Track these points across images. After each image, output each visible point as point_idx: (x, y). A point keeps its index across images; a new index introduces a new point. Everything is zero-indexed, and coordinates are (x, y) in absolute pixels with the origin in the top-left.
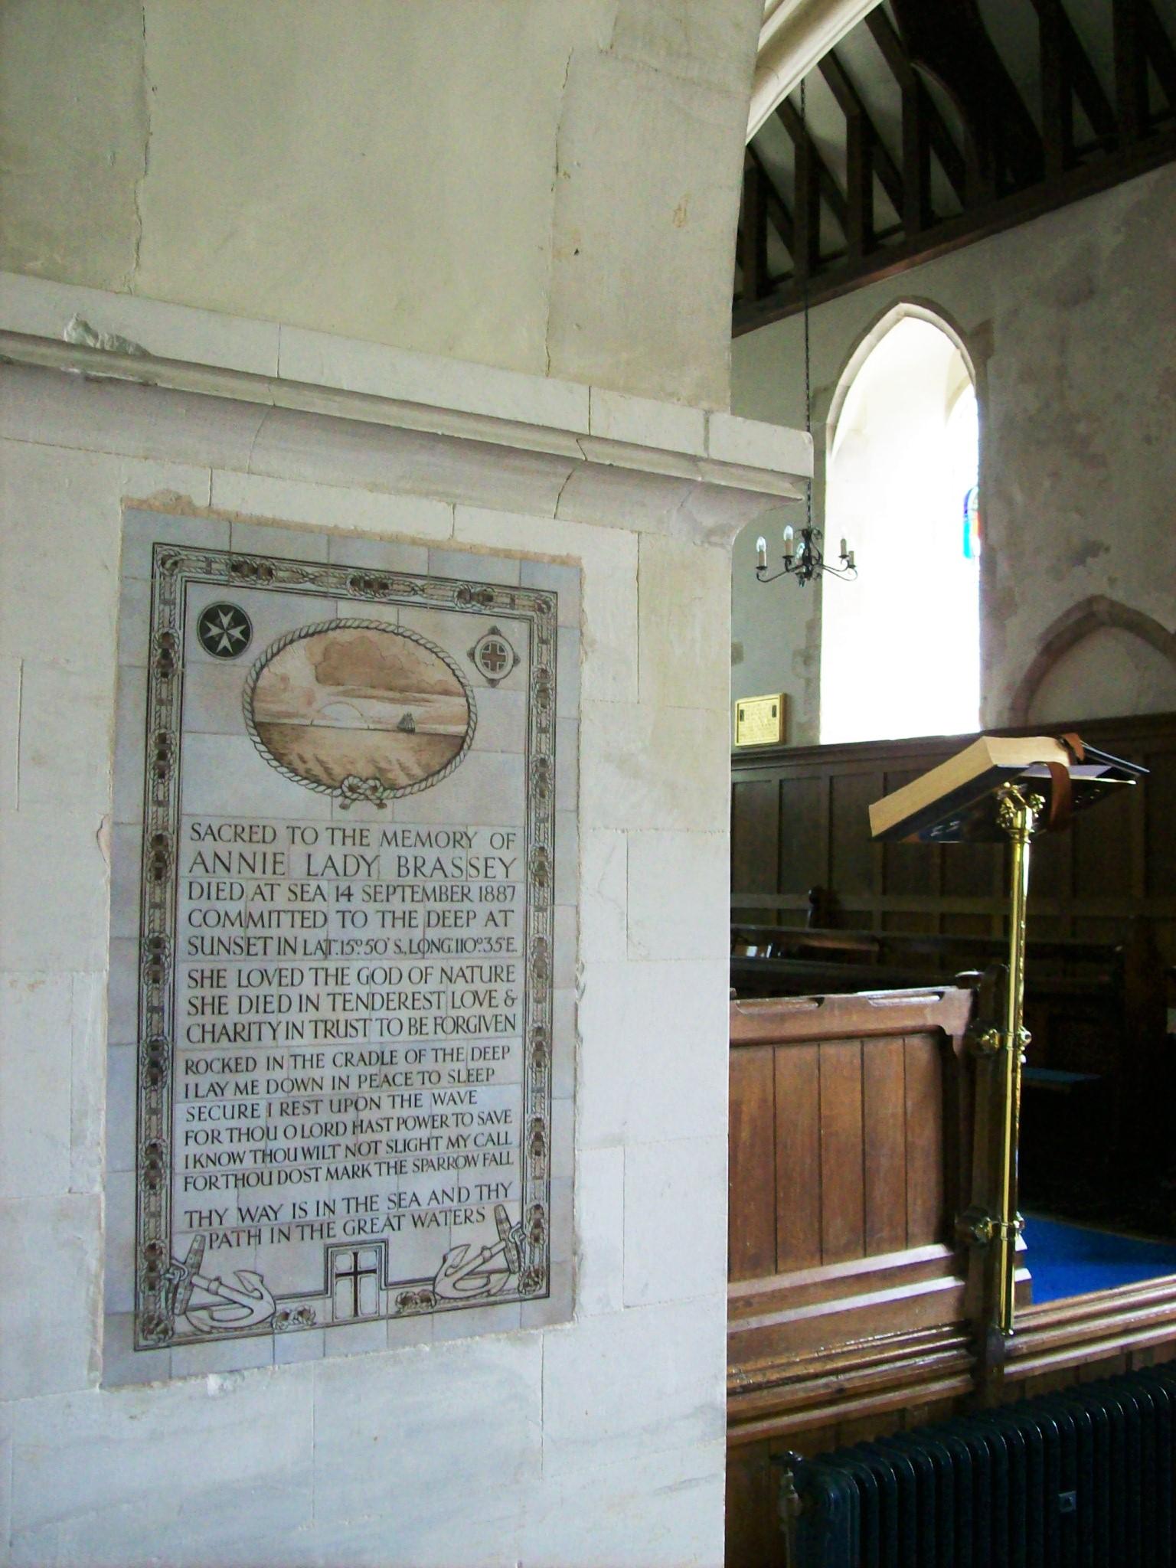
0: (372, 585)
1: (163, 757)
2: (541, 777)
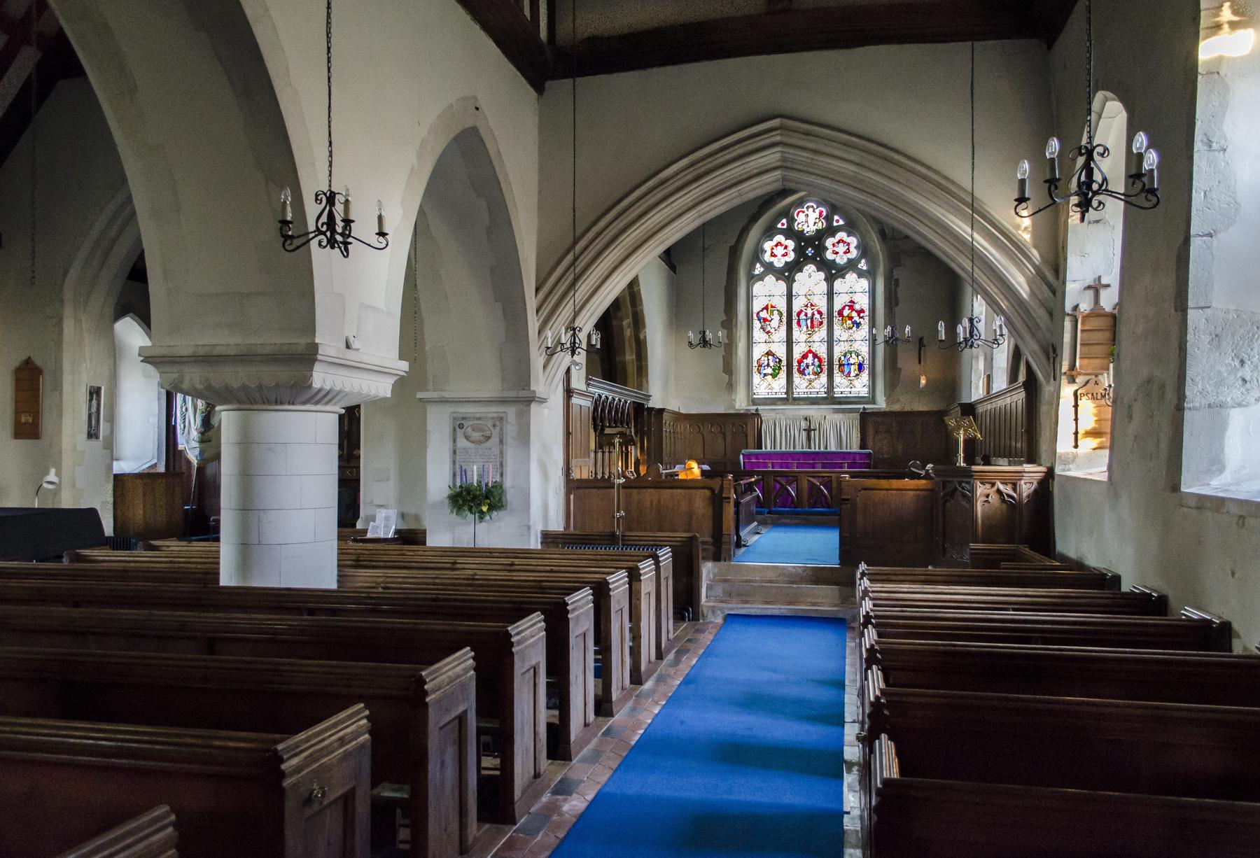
0: (479, 419)
1: (455, 441)
2: (501, 442)
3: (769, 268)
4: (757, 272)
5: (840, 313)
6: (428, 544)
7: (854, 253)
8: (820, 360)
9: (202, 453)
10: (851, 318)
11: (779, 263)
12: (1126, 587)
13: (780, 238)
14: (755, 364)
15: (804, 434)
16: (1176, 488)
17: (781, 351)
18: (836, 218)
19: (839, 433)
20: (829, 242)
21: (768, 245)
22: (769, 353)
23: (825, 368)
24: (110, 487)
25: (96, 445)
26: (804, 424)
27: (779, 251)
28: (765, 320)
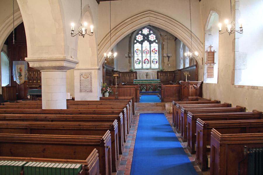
3: (138, 41)
4: (135, 42)
5: (152, 51)
6: (75, 100)
7: (155, 39)
8: (148, 60)
9: (20, 82)
10: (154, 52)
11: (140, 40)
13: (139, 35)
14: (135, 61)
15: (146, 76)
16: (233, 84)
17: (140, 59)
18: (151, 31)
19: (153, 76)
20: (150, 36)
21: (137, 37)
22: (138, 59)
23: (149, 62)
24: (1, 89)
26: (146, 74)
27: (140, 38)
28: (137, 52)
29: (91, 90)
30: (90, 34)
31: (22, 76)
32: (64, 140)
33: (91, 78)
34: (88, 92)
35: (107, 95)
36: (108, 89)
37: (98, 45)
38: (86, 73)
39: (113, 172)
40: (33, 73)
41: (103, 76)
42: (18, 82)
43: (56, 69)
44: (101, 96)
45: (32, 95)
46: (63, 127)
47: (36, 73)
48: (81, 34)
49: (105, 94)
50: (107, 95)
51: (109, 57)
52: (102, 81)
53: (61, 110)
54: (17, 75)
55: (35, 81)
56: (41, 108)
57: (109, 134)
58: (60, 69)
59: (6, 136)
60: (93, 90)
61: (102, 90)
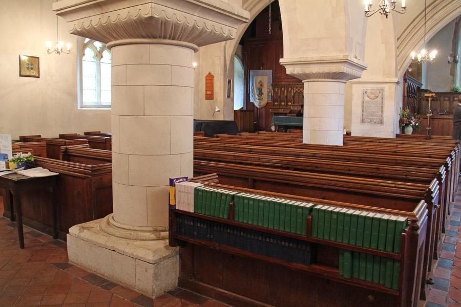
9: (260, 103)
12: (42, 137)
24: (233, 114)
25: (230, 100)
29: (382, 120)
30: (401, 10)
31: (262, 94)
32: (359, 186)
33: (382, 98)
34: (375, 123)
35: (409, 130)
36: (412, 119)
37: (398, 39)
38: (373, 89)
39: (434, 259)
40: (281, 90)
41: (404, 97)
42: (257, 104)
43: (329, 78)
44: (398, 133)
45: (278, 125)
46: (349, 170)
47: (285, 90)
48: (383, 11)
49: (405, 130)
50: (409, 130)
51: (419, 60)
52: (401, 105)
53: (336, 146)
54: (256, 92)
55: (283, 103)
56: (302, 141)
57: (436, 186)
58: (336, 79)
59: (266, 171)
60: (385, 120)
61: (401, 121)
